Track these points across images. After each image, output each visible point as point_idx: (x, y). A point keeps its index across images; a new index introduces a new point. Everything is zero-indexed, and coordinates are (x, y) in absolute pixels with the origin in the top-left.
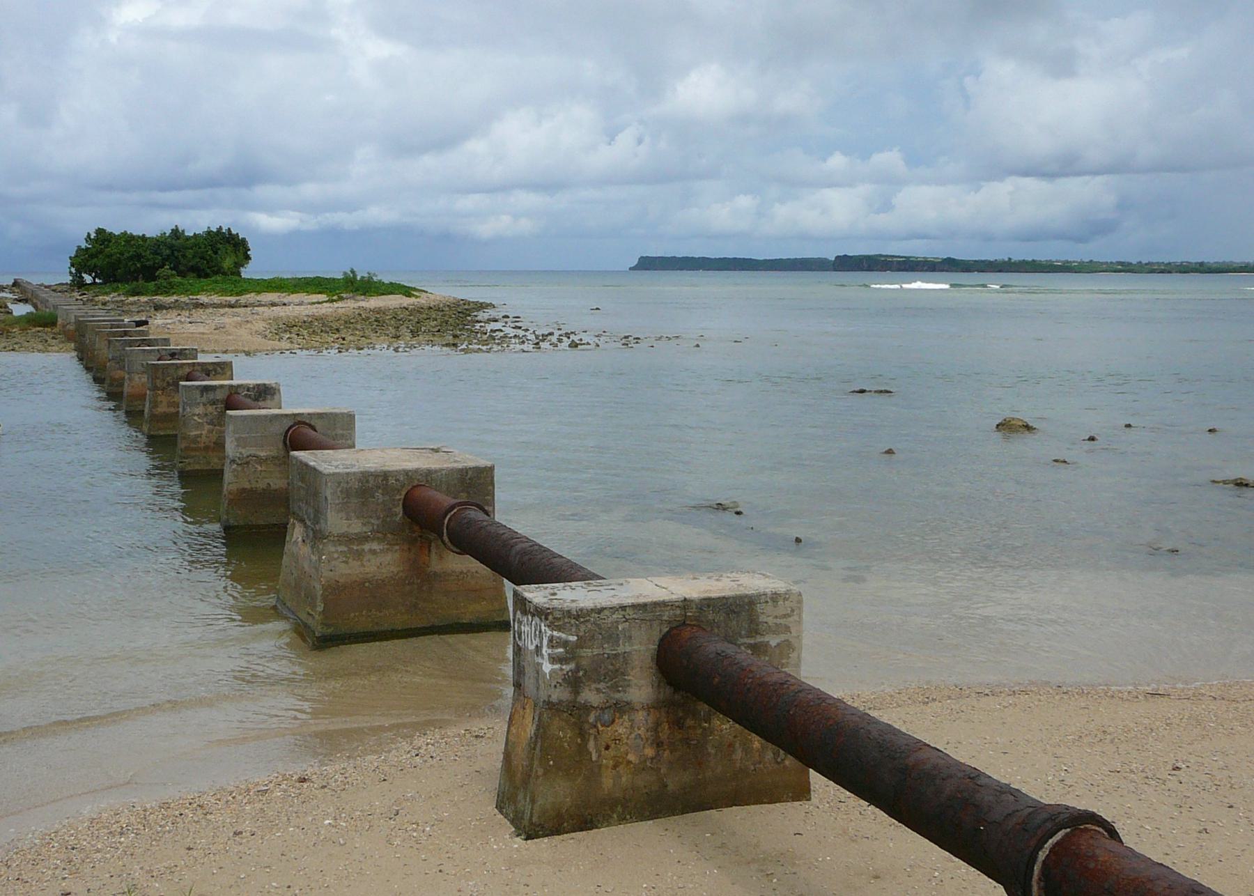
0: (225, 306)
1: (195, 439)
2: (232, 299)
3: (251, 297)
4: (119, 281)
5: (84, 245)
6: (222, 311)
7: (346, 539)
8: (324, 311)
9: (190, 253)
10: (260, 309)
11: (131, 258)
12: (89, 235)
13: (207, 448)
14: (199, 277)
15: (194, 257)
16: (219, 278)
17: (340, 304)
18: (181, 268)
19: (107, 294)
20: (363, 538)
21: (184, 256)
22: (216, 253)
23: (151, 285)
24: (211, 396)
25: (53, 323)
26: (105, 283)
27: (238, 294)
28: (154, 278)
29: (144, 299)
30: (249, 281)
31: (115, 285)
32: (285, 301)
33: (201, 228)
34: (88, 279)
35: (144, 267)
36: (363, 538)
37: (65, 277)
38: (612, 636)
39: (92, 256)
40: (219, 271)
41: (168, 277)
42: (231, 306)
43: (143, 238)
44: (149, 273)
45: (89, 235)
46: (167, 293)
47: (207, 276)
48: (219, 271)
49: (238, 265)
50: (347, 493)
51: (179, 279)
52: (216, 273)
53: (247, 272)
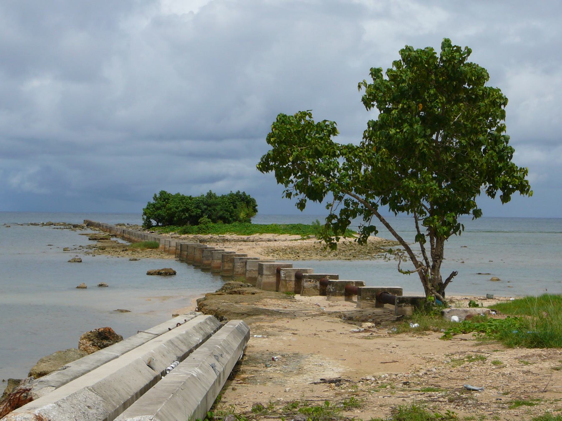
0: (241, 241)
1: (238, 272)
2: (245, 237)
3: (256, 236)
4: (174, 224)
5: (152, 201)
6: (240, 243)
7: (267, 275)
8: (293, 244)
9: (218, 208)
10: (261, 243)
11: (183, 211)
12: (155, 195)
13: (240, 274)
14: (225, 222)
15: (221, 210)
16: (237, 223)
17: (307, 241)
18: (214, 217)
19: (167, 232)
20: (269, 275)
21: (214, 210)
22: (235, 207)
23: (195, 227)
24: (242, 260)
25: (81, 261)
26: (162, 226)
27: (249, 234)
28: (197, 223)
29: (191, 236)
30: (256, 226)
31: (172, 227)
32: (277, 238)
33: (227, 192)
34: (154, 223)
35: (190, 216)
36: (269, 275)
37: (140, 222)
38: (290, 272)
39: (158, 209)
40: (237, 219)
41: (206, 223)
42: (244, 241)
43: (190, 198)
44: (195, 220)
45: (155, 195)
46: (205, 233)
47: (229, 222)
48: (237, 219)
49: (249, 216)
50: (267, 267)
51: (211, 224)
52: (235, 220)
53: (255, 221)
